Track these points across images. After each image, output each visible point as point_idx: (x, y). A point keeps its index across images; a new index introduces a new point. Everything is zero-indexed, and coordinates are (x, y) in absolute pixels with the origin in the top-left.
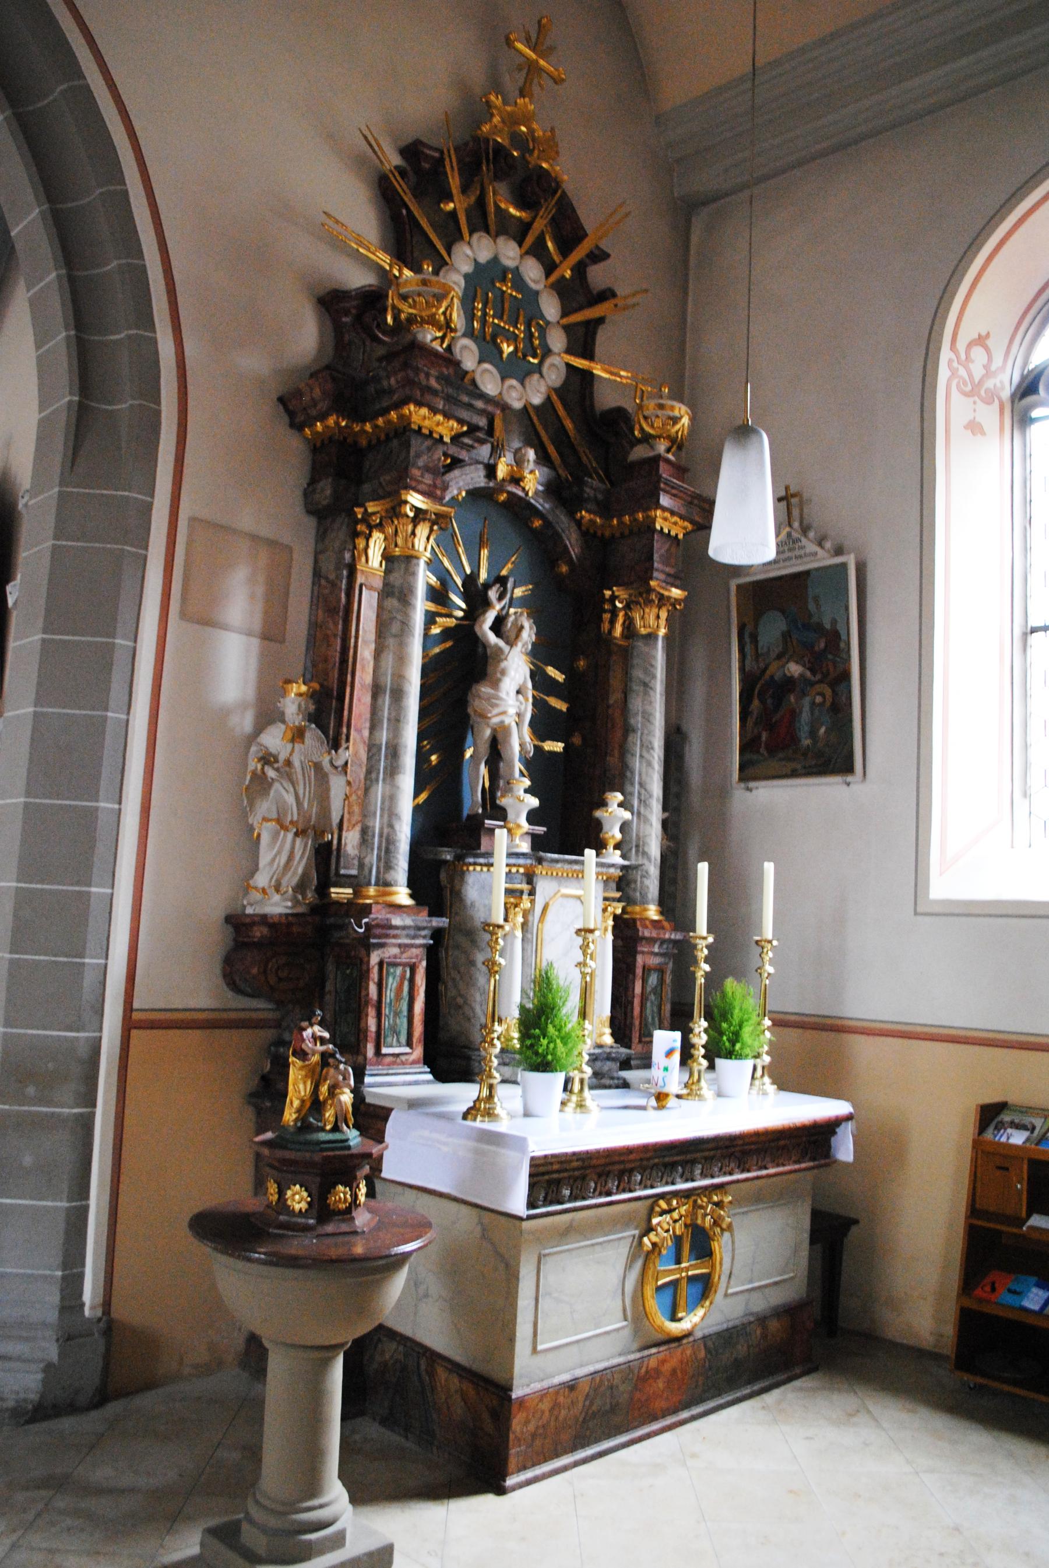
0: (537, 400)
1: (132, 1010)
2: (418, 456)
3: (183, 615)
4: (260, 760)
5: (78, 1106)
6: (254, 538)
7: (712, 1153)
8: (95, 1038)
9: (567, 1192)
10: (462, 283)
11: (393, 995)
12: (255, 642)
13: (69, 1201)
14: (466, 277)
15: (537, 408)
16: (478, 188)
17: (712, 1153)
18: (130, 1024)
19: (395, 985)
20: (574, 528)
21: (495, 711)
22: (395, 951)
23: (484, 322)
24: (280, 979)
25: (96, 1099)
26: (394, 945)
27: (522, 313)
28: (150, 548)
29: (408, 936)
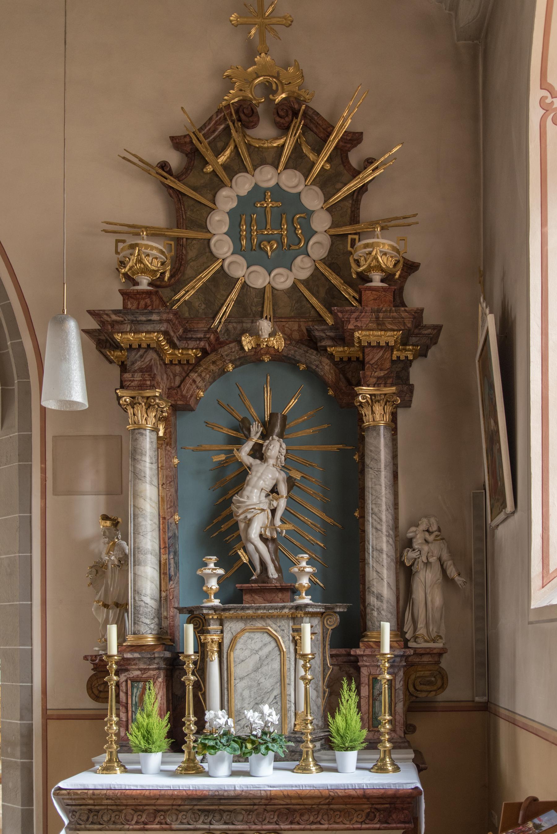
0: (304, 275)
1: (47, 709)
2: (133, 363)
3: (55, 493)
4: (431, 563)
5: (27, 759)
6: (95, 437)
7: (169, 807)
8: (29, 724)
9: (106, 818)
10: (227, 219)
11: (137, 700)
12: (102, 499)
13: (22, 806)
14: (230, 213)
15: (306, 282)
16: (233, 142)
17: (169, 807)
18: (46, 717)
19: (138, 693)
20: (326, 361)
21: (240, 511)
22: (138, 673)
23: (250, 239)
24: (100, 692)
25: (32, 756)
26: (136, 670)
27: (284, 216)
28: (33, 460)
29: (145, 663)
